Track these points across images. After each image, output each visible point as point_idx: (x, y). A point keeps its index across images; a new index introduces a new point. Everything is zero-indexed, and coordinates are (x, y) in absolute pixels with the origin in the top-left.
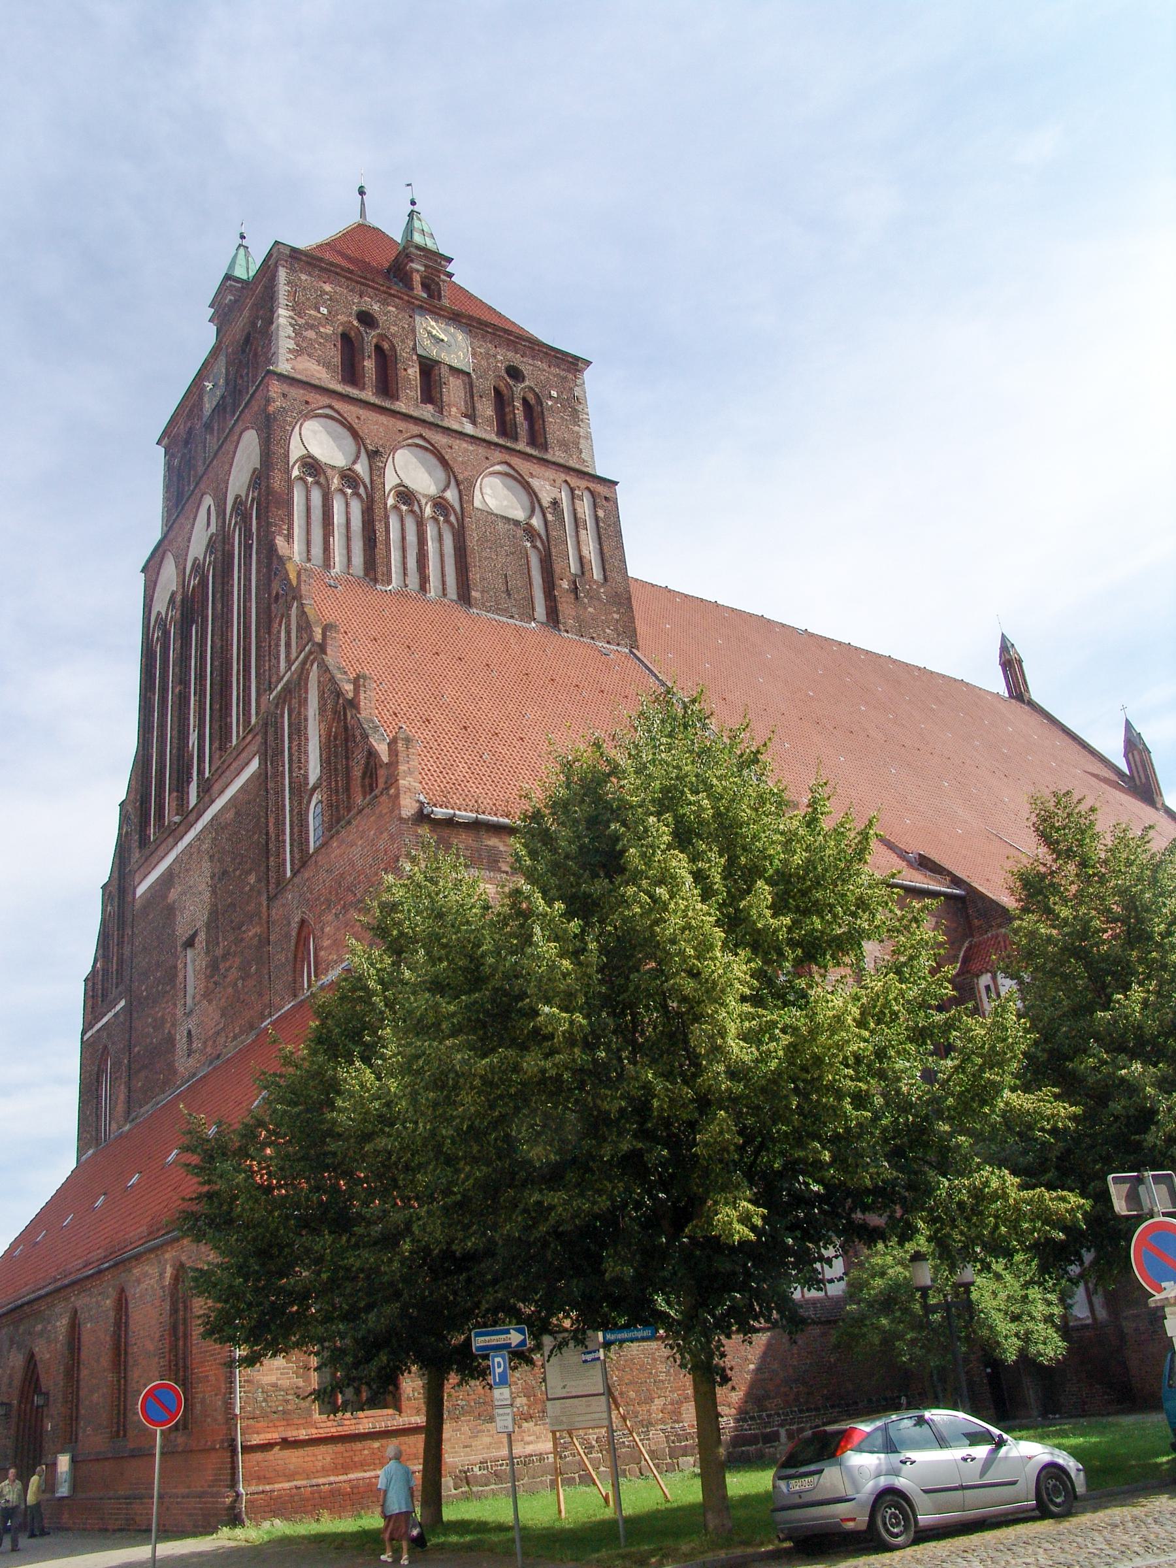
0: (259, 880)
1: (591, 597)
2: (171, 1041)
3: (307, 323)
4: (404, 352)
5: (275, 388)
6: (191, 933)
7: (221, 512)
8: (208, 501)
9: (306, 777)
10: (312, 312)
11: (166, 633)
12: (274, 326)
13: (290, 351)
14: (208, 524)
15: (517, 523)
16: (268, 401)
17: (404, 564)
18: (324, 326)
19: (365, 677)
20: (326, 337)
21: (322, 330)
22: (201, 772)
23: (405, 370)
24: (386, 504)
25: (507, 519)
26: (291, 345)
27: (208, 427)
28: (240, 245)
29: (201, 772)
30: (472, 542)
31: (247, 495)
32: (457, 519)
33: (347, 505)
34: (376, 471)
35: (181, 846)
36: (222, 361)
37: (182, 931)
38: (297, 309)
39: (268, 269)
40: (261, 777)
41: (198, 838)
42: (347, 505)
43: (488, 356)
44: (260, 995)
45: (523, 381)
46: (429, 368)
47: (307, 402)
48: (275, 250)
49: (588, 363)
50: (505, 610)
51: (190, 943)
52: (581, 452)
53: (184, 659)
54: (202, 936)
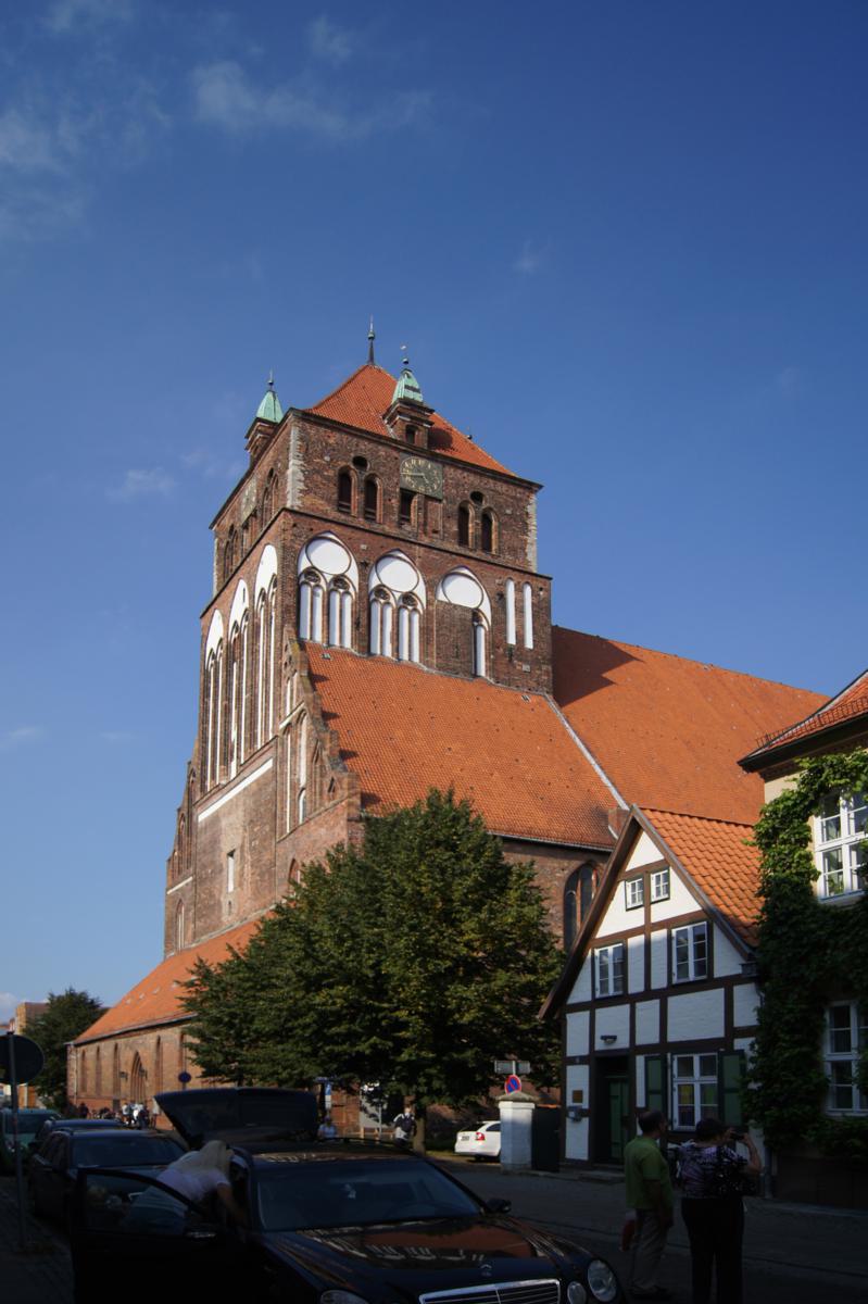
0: (271, 830)
7: (252, 597)
8: (242, 584)
9: (299, 780)
11: (217, 663)
18: (327, 471)
20: (328, 478)
22: (239, 757)
27: (246, 527)
29: (239, 757)
40: (274, 772)
41: (237, 796)
44: (270, 892)
51: (231, 854)
52: (526, 554)
53: (228, 684)
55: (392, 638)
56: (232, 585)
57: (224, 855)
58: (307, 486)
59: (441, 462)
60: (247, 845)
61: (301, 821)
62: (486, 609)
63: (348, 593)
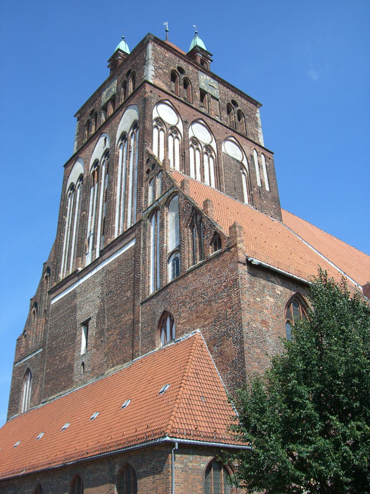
1: (265, 197)
2: (70, 368)
3: (159, 67)
4: (194, 84)
6: (87, 319)
10: (161, 63)
13: (153, 76)
15: (238, 161)
16: (145, 93)
17: (195, 169)
18: (166, 69)
19: (210, 201)
21: (165, 70)
22: (94, 249)
23: (195, 93)
25: (234, 159)
26: (153, 73)
31: (130, 131)
32: (215, 155)
34: (186, 129)
35: (81, 281)
37: (81, 316)
38: (156, 61)
42: (174, 141)
43: (225, 94)
46: (203, 93)
47: (160, 96)
48: (147, 37)
50: (234, 195)
54: (94, 320)
55: (200, 169)
58: (155, 74)
63: (177, 137)
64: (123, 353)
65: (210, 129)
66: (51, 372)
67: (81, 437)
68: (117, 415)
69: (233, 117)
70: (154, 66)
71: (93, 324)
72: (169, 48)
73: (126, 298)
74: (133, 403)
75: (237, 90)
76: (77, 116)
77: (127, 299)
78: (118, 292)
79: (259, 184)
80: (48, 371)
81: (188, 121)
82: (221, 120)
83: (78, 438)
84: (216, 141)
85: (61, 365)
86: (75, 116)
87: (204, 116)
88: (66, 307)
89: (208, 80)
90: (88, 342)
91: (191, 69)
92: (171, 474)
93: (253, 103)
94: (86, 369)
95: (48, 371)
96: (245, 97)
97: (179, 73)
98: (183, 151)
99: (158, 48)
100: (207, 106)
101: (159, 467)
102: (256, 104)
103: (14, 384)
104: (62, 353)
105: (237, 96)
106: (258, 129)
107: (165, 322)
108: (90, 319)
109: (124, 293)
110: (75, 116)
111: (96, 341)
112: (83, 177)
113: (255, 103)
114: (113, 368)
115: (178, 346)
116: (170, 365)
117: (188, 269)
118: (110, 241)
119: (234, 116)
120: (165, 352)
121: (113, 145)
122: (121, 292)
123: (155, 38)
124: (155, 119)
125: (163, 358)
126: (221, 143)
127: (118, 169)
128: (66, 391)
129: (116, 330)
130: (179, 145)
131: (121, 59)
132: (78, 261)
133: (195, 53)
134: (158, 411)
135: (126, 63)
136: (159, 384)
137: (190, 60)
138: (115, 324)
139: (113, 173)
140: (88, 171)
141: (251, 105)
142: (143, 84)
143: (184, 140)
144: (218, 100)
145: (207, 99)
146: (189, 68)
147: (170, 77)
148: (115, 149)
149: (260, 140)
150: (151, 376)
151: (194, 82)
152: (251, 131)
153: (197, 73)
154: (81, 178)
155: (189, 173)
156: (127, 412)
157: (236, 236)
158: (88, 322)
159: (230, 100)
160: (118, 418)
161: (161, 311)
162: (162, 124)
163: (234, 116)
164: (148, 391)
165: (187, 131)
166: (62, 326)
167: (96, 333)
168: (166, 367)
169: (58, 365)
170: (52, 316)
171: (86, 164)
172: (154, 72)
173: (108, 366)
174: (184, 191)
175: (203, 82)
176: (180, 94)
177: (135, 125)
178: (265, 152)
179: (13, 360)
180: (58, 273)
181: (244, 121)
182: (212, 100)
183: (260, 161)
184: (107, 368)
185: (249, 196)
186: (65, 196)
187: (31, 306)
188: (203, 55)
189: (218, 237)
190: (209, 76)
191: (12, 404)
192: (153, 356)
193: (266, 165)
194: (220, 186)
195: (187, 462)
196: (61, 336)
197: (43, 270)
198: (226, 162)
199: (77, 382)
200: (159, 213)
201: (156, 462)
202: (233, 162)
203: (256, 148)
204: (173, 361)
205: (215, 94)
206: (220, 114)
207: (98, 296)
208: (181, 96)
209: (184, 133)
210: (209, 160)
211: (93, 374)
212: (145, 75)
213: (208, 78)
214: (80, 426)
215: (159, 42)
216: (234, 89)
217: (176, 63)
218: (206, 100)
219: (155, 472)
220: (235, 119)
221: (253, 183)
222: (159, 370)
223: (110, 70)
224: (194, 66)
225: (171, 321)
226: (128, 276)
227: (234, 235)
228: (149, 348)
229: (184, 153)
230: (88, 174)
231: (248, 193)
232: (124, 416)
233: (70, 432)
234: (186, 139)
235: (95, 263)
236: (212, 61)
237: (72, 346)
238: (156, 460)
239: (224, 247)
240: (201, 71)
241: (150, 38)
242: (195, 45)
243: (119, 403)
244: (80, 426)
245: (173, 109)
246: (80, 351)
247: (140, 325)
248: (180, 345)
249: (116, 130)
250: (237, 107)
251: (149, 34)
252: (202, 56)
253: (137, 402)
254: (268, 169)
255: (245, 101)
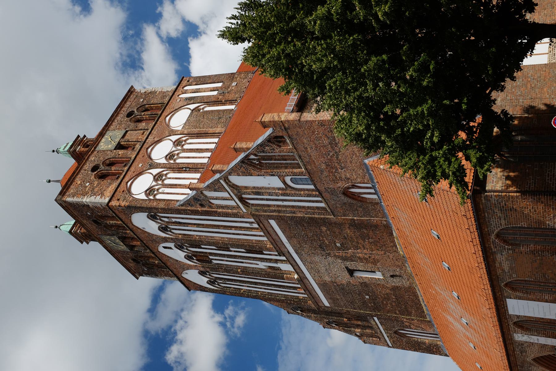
2: (395, 289)
3: (91, 191)
4: (110, 155)
5: (114, 203)
10: (87, 189)
12: (90, 205)
13: (101, 197)
14: (170, 248)
17: (199, 158)
18: (94, 184)
20: (98, 185)
22: (276, 261)
23: (119, 155)
24: (172, 163)
26: (98, 197)
28: (59, 228)
30: (196, 130)
31: (159, 223)
32: (185, 137)
33: (170, 178)
34: (158, 166)
36: (106, 238)
37: (344, 278)
38: (84, 194)
39: (69, 208)
42: (170, 178)
45: (133, 111)
46: (119, 146)
48: (59, 202)
49: (132, 87)
51: (351, 272)
55: (199, 152)
56: (164, 259)
57: (352, 280)
58: (99, 195)
59: (107, 131)
60: (341, 253)
61: (312, 187)
62: (193, 106)
63: (166, 175)
64: (383, 235)
65: (158, 141)
66: (399, 309)
67: (467, 280)
68: (446, 243)
69: (144, 116)
70: (91, 196)
71: (351, 265)
72: (71, 180)
73: (328, 231)
74: (435, 228)
75: (116, 111)
76: (138, 276)
77: (329, 230)
78: (321, 238)
79: (215, 93)
80: (398, 312)
81: (150, 163)
82: (147, 130)
83: (468, 283)
84: (171, 136)
85: (392, 298)
86: (137, 278)
87: (144, 146)
88: (333, 292)
89: (105, 141)
90: (370, 270)
91: (94, 158)
92: (508, 194)
93: (130, 95)
94: (398, 274)
95: (398, 312)
96: (123, 103)
97: (99, 170)
98: (181, 169)
99: (72, 190)
100: (133, 143)
101: (500, 205)
102: (131, 92)
103: (410, 347)
104: (380, 297)
105: (122, 112)
106: (157, 91)
107: (353, 194)
108: (347, 268)
109: (323, 233)
110: (137, 278)
111: (369, 262)
112: (202, 272)
113: (129, 94)
114: (398, 246)
115: (379, 182)
116: (398, 190)
117: (303, 169)
118: (269, 245)
119: (143, 115)
120: (385, 194)
121: (171, 240)
122: (322, 236)
123: (60, 194)
124: (147, 197)
125: (390, 196)
126: (172, 130)
127: (197, 235)
128: (419, 295)
129: (360, 242)
130: (174, 173)
131: (80, 230)
132: (288, 278)
133: (76, 153)
134: (445, 203)
135: (86, 225)
136: (417, 202)
137: (84, 159)
138: (353, 243)
139: (201, 241)
140: (196, 265)
141: (131, 97)
142: (110, 208)
143: (169, 168)
144: (127, 132)
145: (125, 143)
146: (93, 159)
147: (102, 180)
148: (176, 238)
149: (169, 90)
150: (408, 209)
151: (108, 155)
152: (159, 99)
153: (98, 152)
154: (202, 273)
155: (203, 164)
156: (443, 234)
157: (273, 121)
158: (350, 269)
159: (126, 119)
160: (449, 243)
161: (343, 197)
162: (152, 190)
163: (143, 115)
164: (424, 213)
165: (160, 165)
166: (352, 296)
167: (361, 262)
168: (399, 194)
169: (393, 302)
170: (342, 306)
171: (189, 267)
172: (98, 196)
173: (395, 251)
174: (224, 170)
175: (108, 146)
176: (121, 170)
177: (153, 217)
178: (181, 86)
179: (386, 348)
180: (299, 299)
181: (149, 106)
182: (126, 138)
183: (191, 91)
184: (397, 252)
185: (227, 104)
186: (220, 290)
187: (331, 328)
188: (79, 145)
189: (273, 139)
190: (101, 139)
191: (430, 350)
192: (388, 206)
193: (195, 85)
194: (217, 133)
195: (496, 177)
196: (363, 298)
197: (295, 314)
198: (192, 126)
199: (410, 283)
200: (244, 196)
201: (496, 207)
202: (192, 119)
203: (177, 95)
204: (394, 187)
205: (120, 134)
206: (142, 130)
207: (325, 258)
208: (122, 170)
209: (162, 168)
210: (190, 143)
211: (403, 266)
212: (100, 206)
213: (103, 140)
214: (456, 281)
215: (65, 191)
216: (115, 115)
217: (88, 173)
218: (127, 144)
219: (506, 209)
220: (147, 115)
221: (213, 99)
222: (402, 201)
223: (91, 242)
224: (90, 155)
225: (353, 188)
226: (306, 229)
227: (272, 123)
228: (379, 210)
229: (183, 168)
230: (200, 267)
231: (224, 105)
232: (448, 237)
233: (462, 291)
234: (168, 166)
235: (290, 260)
236: (85, 136)
237: (373, 287)
238: (493, 207)
239: (284, 134)
240: (95, 148)
241: (60, 200)
242: (67, 153)
243: (434, 241)
244: (456, 281)
245: (137, 178)
246: (379, 279)
247: (355, 218)
248: (378, 179)
249: (156, 237)
250: (134, 112)
251: (56, 200)
252: (80, 146)
253: (434, 224)
254: (199, 83)
255: (127, 103)
